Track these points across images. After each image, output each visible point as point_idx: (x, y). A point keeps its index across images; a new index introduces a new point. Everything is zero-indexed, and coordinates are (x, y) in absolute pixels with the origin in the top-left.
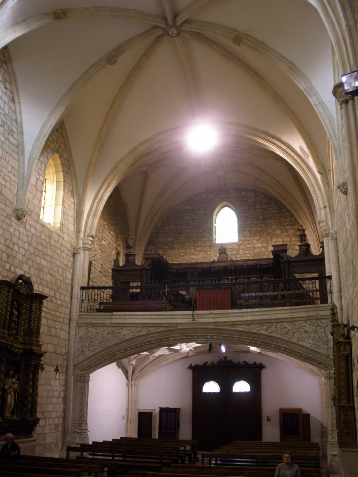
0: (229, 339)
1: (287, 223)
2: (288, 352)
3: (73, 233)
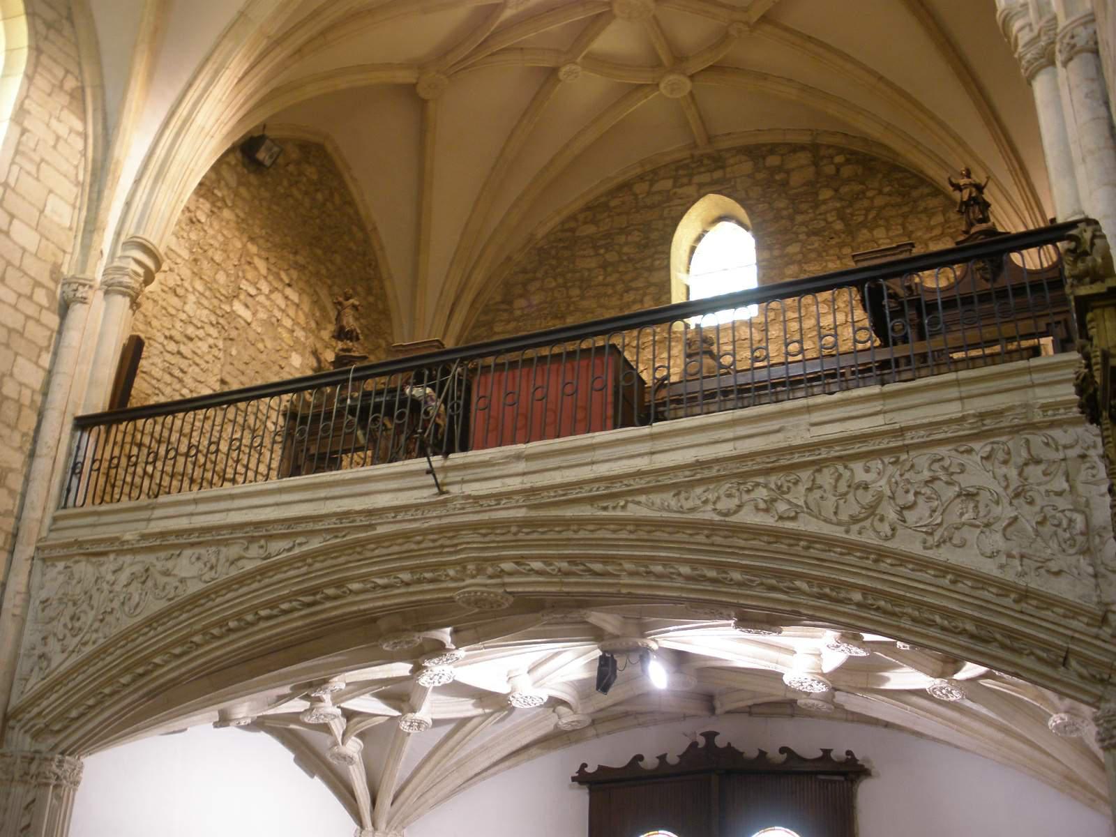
0: (598, 567)
1: (937, 232)
2: (885, 612)
3: (72, 234)
